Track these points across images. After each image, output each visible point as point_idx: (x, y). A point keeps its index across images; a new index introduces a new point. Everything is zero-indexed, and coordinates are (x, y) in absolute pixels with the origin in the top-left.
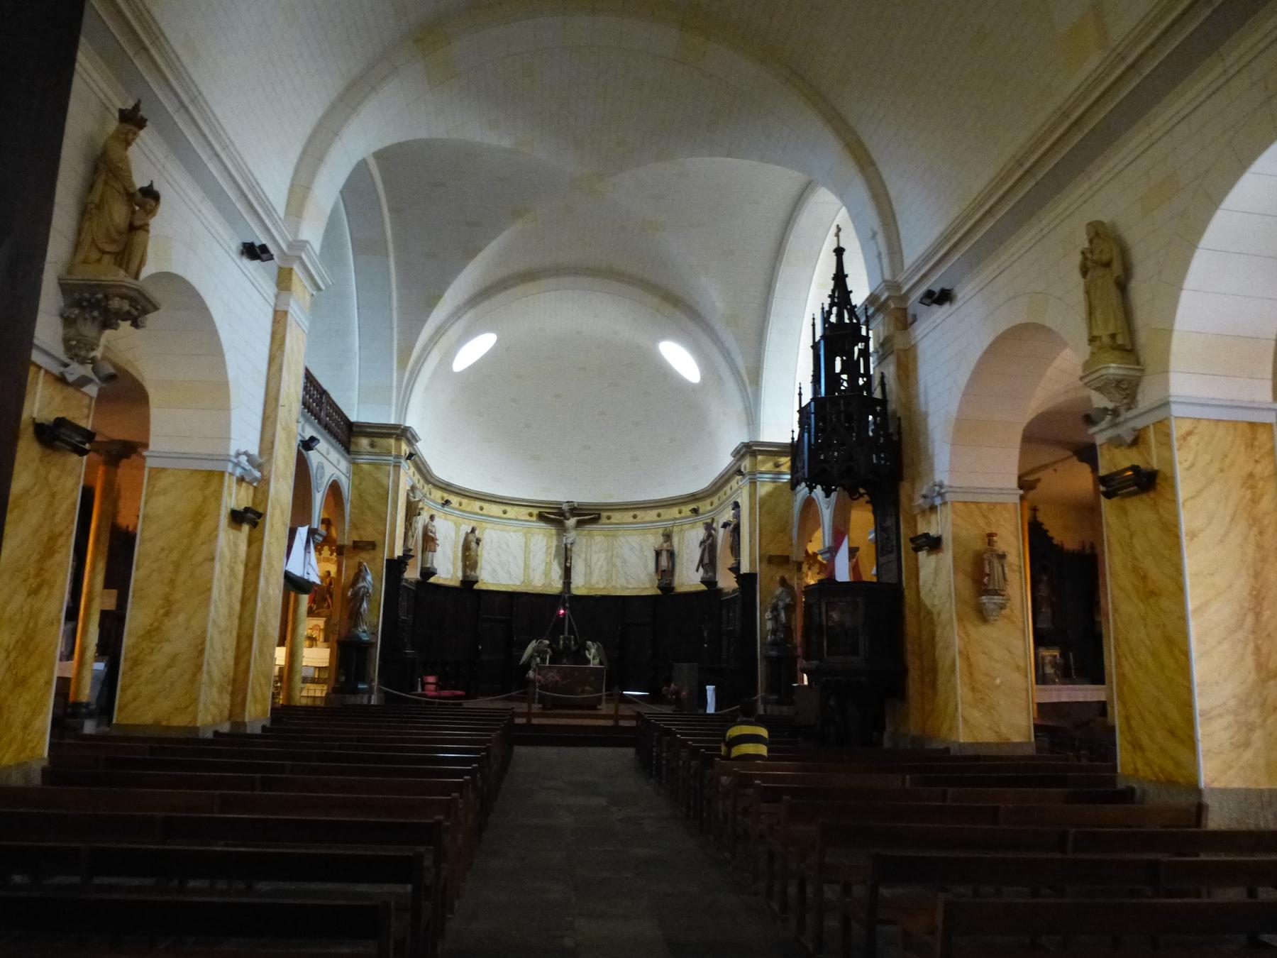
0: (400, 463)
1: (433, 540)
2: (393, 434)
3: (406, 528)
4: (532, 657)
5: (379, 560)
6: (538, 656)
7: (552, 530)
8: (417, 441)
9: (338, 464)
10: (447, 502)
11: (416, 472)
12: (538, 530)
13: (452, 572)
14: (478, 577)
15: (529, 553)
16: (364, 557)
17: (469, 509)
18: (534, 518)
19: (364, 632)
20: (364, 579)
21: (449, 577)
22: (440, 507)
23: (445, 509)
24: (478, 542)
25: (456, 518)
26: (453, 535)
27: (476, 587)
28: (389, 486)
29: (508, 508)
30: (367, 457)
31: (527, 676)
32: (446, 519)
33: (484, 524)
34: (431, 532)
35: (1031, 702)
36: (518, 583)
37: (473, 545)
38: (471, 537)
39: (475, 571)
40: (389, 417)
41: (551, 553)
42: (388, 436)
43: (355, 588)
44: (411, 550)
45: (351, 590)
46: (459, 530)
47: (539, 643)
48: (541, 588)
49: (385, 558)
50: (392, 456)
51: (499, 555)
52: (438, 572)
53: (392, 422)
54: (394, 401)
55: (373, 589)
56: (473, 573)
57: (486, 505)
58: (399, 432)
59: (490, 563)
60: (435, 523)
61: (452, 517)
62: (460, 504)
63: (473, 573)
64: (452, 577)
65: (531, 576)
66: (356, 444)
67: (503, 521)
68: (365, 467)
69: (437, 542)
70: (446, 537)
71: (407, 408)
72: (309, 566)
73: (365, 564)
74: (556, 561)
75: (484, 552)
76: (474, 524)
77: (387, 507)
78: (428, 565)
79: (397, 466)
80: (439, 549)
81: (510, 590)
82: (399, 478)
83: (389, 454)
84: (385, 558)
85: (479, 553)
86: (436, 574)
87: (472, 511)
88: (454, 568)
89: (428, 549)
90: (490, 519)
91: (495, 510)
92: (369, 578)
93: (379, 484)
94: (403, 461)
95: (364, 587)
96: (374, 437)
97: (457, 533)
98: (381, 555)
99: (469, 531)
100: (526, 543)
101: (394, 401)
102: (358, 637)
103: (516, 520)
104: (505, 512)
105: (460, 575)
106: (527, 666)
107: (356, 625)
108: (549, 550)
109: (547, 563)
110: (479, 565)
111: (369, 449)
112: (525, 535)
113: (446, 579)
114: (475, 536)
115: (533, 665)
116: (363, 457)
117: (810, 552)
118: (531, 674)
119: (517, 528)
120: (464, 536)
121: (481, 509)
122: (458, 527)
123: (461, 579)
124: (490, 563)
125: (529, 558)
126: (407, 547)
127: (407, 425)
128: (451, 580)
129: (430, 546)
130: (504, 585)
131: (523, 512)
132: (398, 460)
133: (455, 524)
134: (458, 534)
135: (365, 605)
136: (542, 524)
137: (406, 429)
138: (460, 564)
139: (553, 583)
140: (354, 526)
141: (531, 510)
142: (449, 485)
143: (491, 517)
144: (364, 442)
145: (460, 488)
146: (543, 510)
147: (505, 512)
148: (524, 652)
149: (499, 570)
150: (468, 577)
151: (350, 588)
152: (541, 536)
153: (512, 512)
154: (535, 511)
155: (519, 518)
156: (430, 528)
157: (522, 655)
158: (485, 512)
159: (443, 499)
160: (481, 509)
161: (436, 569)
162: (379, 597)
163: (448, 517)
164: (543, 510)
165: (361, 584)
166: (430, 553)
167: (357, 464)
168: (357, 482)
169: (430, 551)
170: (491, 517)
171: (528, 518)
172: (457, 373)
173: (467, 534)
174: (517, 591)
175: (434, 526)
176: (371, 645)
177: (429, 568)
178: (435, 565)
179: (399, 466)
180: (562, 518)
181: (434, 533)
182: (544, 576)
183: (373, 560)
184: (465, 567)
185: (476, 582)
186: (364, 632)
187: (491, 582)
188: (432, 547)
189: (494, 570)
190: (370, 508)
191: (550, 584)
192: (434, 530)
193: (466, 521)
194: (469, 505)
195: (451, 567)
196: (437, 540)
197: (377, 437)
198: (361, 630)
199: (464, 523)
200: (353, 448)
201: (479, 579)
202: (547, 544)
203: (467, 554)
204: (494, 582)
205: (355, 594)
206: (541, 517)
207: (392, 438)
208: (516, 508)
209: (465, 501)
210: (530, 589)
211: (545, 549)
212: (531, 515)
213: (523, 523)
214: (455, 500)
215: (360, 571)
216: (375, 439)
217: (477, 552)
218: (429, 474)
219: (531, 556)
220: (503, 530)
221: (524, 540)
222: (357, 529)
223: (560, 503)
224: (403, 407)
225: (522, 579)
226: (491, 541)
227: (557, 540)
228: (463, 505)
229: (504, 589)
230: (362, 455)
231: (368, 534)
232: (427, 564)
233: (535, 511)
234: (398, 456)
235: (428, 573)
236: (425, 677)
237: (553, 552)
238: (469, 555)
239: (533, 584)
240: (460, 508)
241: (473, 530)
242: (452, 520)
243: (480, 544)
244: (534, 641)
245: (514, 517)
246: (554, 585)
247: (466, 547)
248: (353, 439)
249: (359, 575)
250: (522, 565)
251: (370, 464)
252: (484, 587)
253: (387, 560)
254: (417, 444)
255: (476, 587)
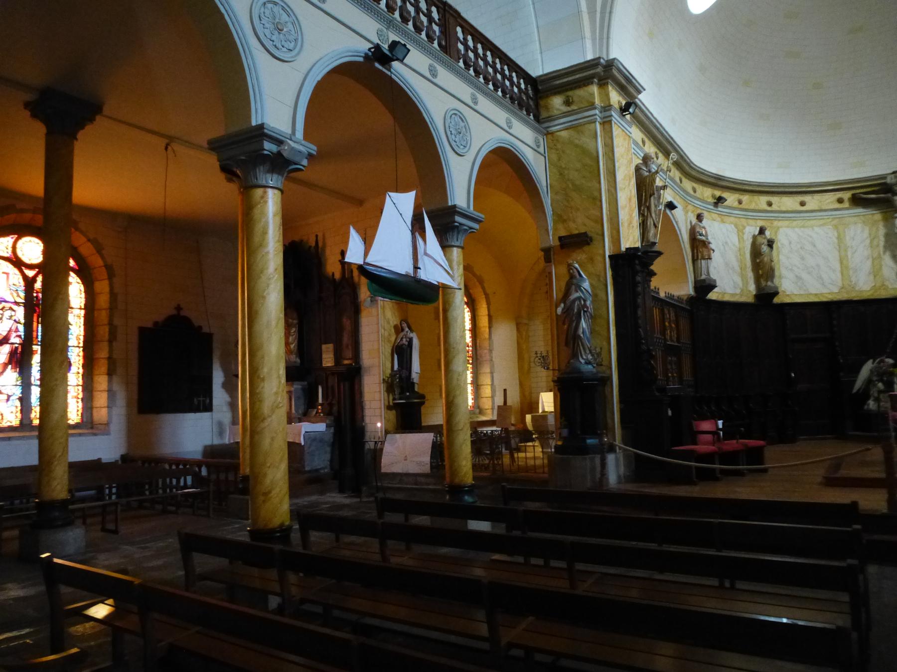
0: (611, 116)
1: (705, 244)
2: (592, 77)
3: (641, 214)
4: (869, 382)
5: (599, 258)
6: (879, 381)
7: (875, 215)
8: (639, 92)
9: (510, 127)
10: (720, 200)
11: (646, 140)
12: (855, 219)
13: (741, 285)
14: (776, 288)
15: (846, 251)
16: (577, 259)
17: (753, 206)
18: (846, 204)
19: (588, 363)
20: (579, 288)
21: (738, 291)
22: (712, 207)
23: (720, 209)
24: (770, 244)
25: (736, 219)
26: (735, 239)
27: (776, 300)
28: (597, 152)
29: (807, 198)
30: (562, 121)
31: (866, 407)
32: (723, 222)
33: (776, 223)
34: (701, 235)
35: (381, 345)
36: (836, 290)
37: (765, 248)
38: (760, 240)
39: (772, 282)
40: (584, 53)
41: (878, 246)
42: (585, 82)
43: (568, 303)
44: (654, 244)
45: (562, 305)
46: (743, 234)
47: (879, 363)
48: (871, 292)
49: (607, 254)
50: (595, 108)
51: (803, 258)
52: (718, 284)
53: (590, 57)
54: (587, 33)
55: (593, 302)
56: (769, 283)
57: (775, 199)
58: (599, 70)
59: (791, 270)
60: (705, 222)
61: (732, 219)
62: (740, 202)
63: (769, 283)
64: (742, 290)
65: (854, 279)
66: (547, 108)
67: (802, 215)
68: (564, 134)
69: (712, 246)
70: (726, 243)
71: (608, 38)
72: (426, 258)
73: (577, 265)
74: (888, 253)
75: (781, 257)
76: (761, 223)
77: (600, 182)
78: (703, 277)
79: (607, 123)
80: (715, 256)
81: (824, 300)
82: (612, 138)
83: (592, 106)
84: (607, 254)
85: (775, 258)
86: (714, 287)
87: (757, 208)
88: (742, 280)
89: (700, 257)
90: (783, 215)
91: (789, 203)
92: (586, 285)
93: (584, 152)
94: (615, 115)
95: (579, 298)
96: (567, 90)
97: (741, 239)
98: (601, 252)
99: (757, 233)
100: (839, 238)
101: (587, 33)
102: (579, 371)
103: (821, 211)
104: (803, 204)
105: (752, 288)
106: (865, 394)
107: (575, 355)
108: (875, 243)
109: (874, 259)
110: (777, 273)
111: (565, 109)
112: (836, 227)
113: (733, 295)
114: (765, 238)
115: (874, 392)
116: (557, 122)
117: (227, 560)
118: (872, 404)
119: (822, 222)
120: (751, 240)
121: (770, 204)
122: (740, 231)
123: (754, 293)
124: (791, 270)
125: (847, 256)
126: (648, 241)
127: (611, 57)
128: (741, 295)
129: (702, 253)
130: (816, 295)
131: (829, 200)
132: (607, 114)
133: (736, 226)
134: (743, 238)
135: (583, 324)
136: (860, 210)
137: (611, 65)
138: (750, 275)
139: (887, 283)
140: (560, 218)
141: (839, 195)
142: (719, 178)
143: (784, 212)
144: (557, 102)
145: (735, 182)
146: (858, 191)
147: (803, 204)
148: (856, 377)
149: (805, 276)
150: (763, 289)
151: (560, 303)
152: (860, 225)
153: (813, 202)
154: (847, 195)
155: (823, 208)
156: (698, 229)
157: (855, 381)
158: (774, 207)
159: (713, 196)
160: (770, 204)
161: (715, 281)
162: (604, 309)
163: (726, 219)
164: (858, 191)
165: (575, 295)
166: (703, 262)
167: (552, 133)
168: (554, 157)
169: (703, 258)
170: (784, 212)
171: (838, 206)
172: (697, 16)
173: (754, 237)
174: (835, 299)
175: (704, 228)
176: (606, 380)
177: (704, 280)
178: (714, 275)
179: (610, 121)
180: (889, 195)
181: (706, 236)
182: (872, 277)
183: (591, 260)
184: (758, 279)
185: (776, 293)
186: (588, 363)
187: (795, 293)
188: (705, 253)
189: (799, 278)
190: (578, 189)
191: (883, 285)
192: (704, 233)
193: (751, 222)
194: (751, 202)
195: (739, 280)
196: (709, 243)
197: (571, 89)
198: (583, 361)
199: (748, 225)
200: (544, 114)
201: (780, 290)
202: (870, 234)
203: (758, 261)
204: (802, 292)
205: (568, 311)
206: (857, 201)
207: (592, 83)
208: (817, 197)
209: (745, 198)
210: (854, 296)
211: (868, 241)
212: (840, 201)
213: (830, 213)
214: (731, 198)
215: (572, 277)
216: (570, 93)
217: (771, 256)
218: (685, 161)
219: (849, 254)
220: (803, 227)
221: (836, 234)
222: (564, 221)
223: (884, 177)
224: (604, 34)
225: (840, 284)
226: (790, 243)
227: (886, 226)
228: (744, 203)
229: (816, 300)
230: (555, 120)
231: (577, 226)
232: (701, 275)
233: (847, 195)
234: (607, 108)
235: (704, 286)
236: (694, 423)
237: (882, 243)
238: (760, 262)
239: (857, 289)
240: (741, 206)
241: (762, 231)
242: (731, 223)
243: (774, 246)
244: (871, 361)
245: (817, 208)
246: (890, 287)
247: (756, 253)
248: (542, 103)
249: (572, 282)
250: (837, 266)
251: (567, 129)
252: (787, 300)
253: (610, 257)
254: (640, 96)
255: (776, 300)
